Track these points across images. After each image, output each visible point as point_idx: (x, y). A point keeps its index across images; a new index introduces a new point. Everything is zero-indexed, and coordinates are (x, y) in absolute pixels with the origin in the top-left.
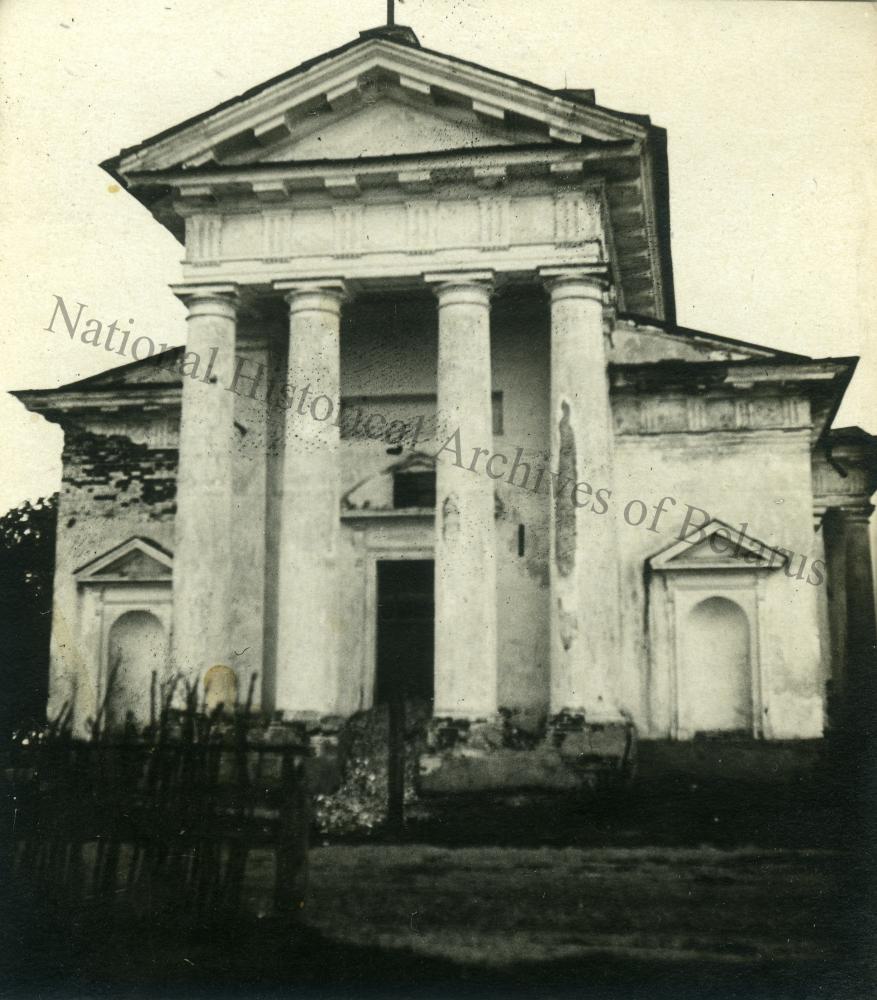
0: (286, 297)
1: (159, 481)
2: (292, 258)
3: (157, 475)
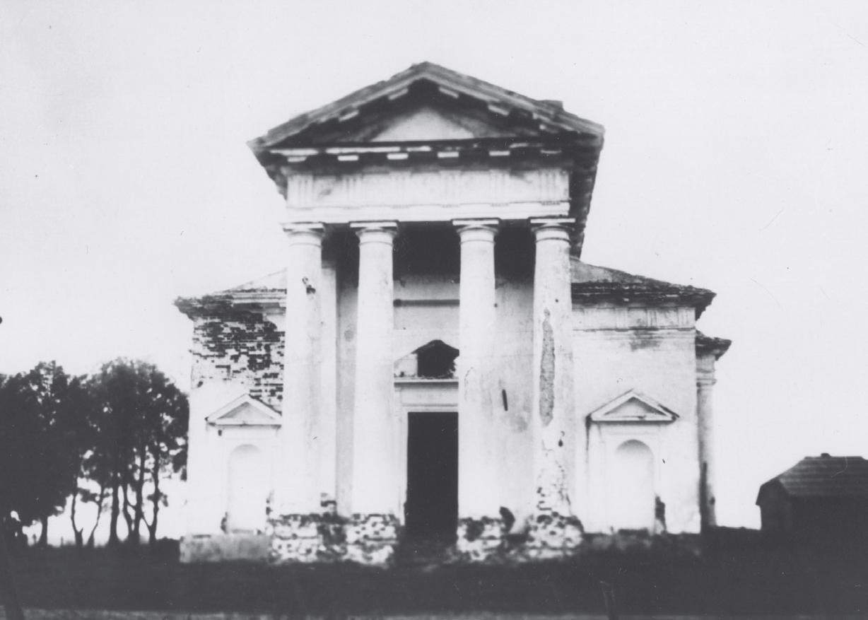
0: (357, 233)
1: (259, 356)
2: (362, 206)
3: (257, 352)
